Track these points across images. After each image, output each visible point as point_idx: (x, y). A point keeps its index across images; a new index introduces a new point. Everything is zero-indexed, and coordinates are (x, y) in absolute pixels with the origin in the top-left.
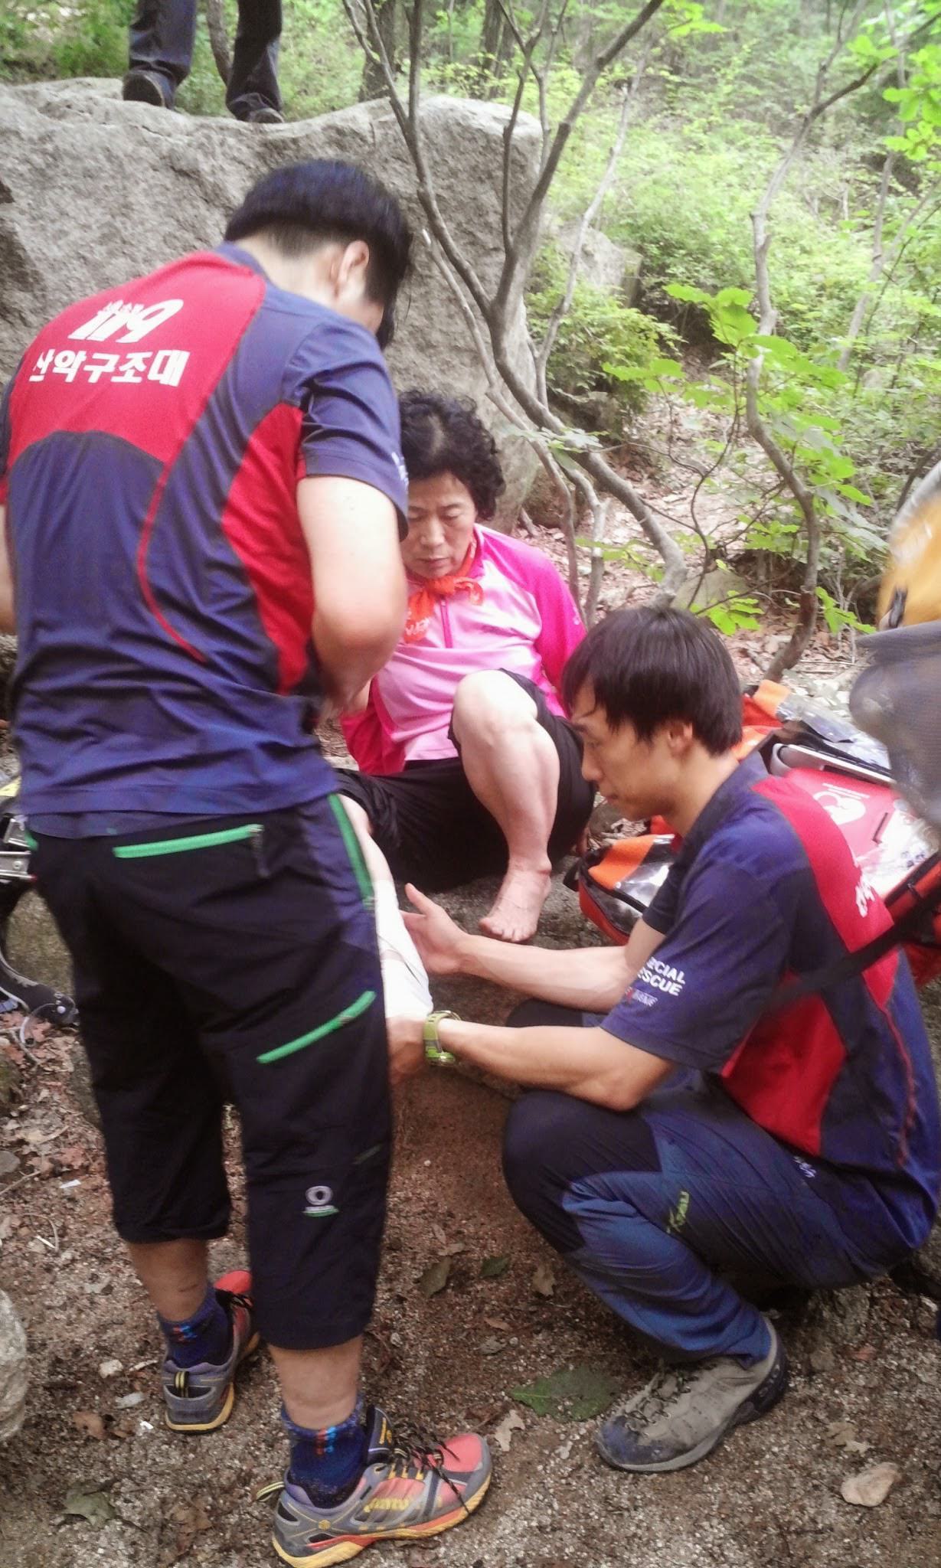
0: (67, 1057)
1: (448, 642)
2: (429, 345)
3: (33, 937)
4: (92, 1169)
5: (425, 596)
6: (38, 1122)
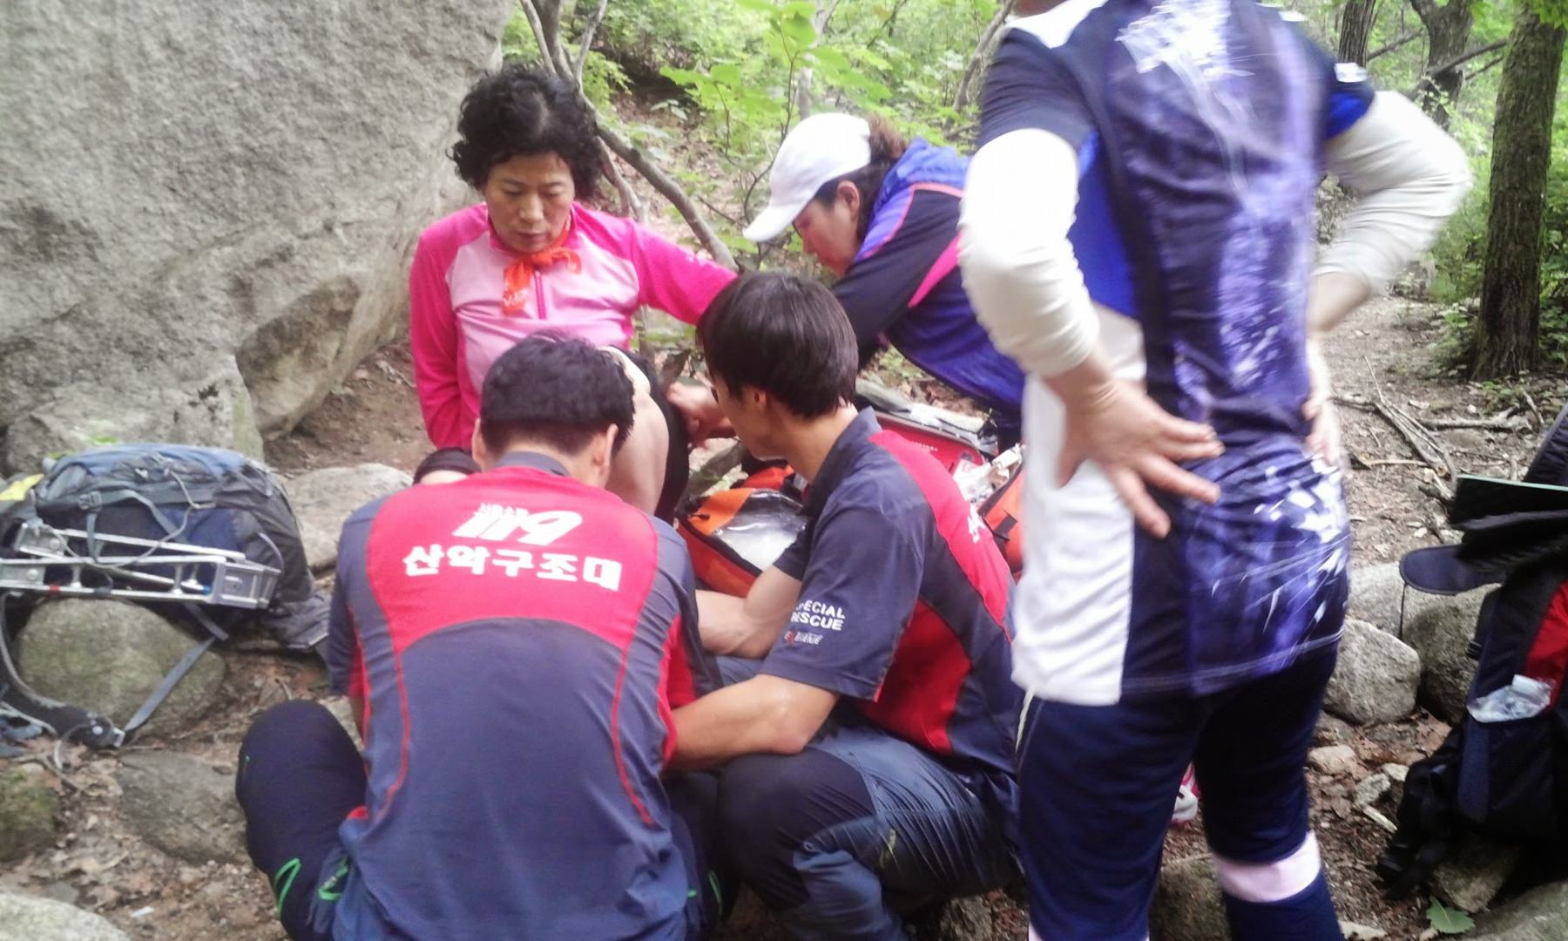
0: (112, 780)
1: (542, 314)
2: (424, 52)
3: (54, 654)
4: (164, 894)
5: (522, 269)
6: (91, 850)
